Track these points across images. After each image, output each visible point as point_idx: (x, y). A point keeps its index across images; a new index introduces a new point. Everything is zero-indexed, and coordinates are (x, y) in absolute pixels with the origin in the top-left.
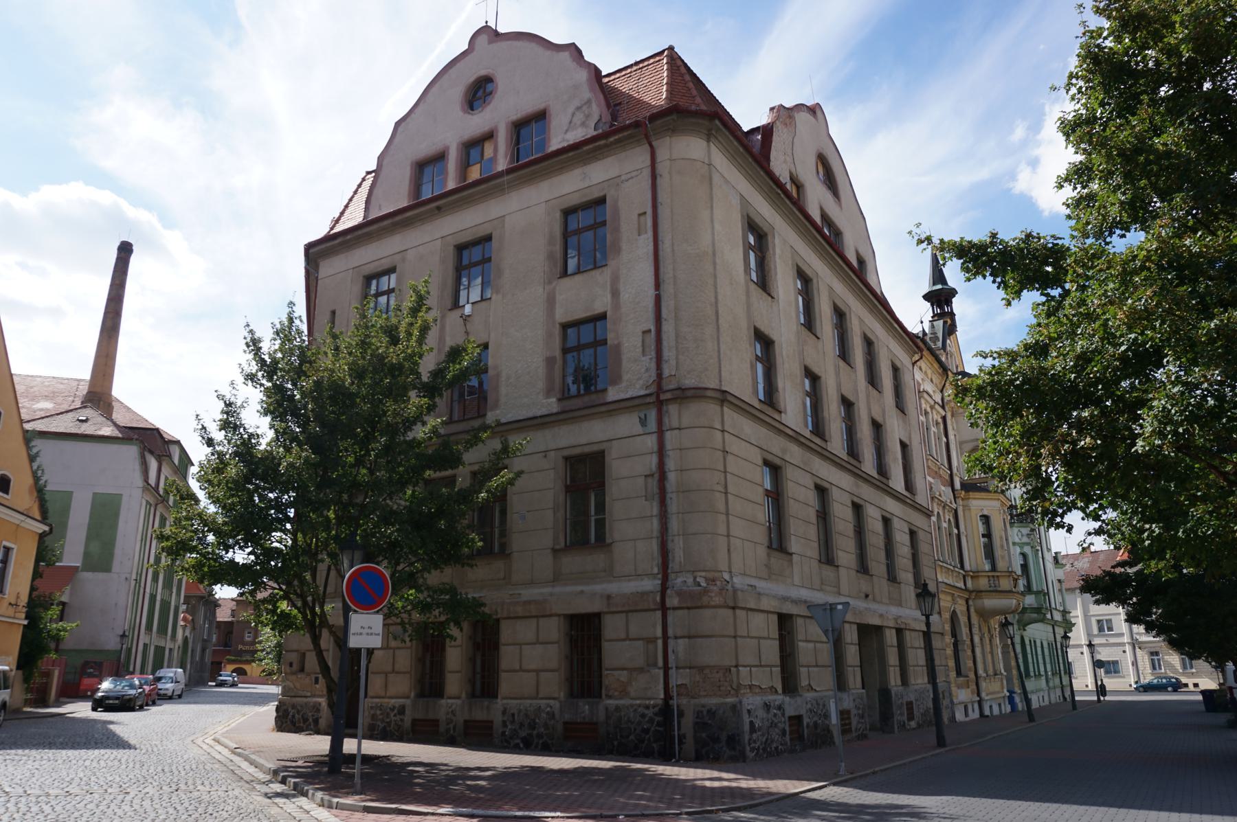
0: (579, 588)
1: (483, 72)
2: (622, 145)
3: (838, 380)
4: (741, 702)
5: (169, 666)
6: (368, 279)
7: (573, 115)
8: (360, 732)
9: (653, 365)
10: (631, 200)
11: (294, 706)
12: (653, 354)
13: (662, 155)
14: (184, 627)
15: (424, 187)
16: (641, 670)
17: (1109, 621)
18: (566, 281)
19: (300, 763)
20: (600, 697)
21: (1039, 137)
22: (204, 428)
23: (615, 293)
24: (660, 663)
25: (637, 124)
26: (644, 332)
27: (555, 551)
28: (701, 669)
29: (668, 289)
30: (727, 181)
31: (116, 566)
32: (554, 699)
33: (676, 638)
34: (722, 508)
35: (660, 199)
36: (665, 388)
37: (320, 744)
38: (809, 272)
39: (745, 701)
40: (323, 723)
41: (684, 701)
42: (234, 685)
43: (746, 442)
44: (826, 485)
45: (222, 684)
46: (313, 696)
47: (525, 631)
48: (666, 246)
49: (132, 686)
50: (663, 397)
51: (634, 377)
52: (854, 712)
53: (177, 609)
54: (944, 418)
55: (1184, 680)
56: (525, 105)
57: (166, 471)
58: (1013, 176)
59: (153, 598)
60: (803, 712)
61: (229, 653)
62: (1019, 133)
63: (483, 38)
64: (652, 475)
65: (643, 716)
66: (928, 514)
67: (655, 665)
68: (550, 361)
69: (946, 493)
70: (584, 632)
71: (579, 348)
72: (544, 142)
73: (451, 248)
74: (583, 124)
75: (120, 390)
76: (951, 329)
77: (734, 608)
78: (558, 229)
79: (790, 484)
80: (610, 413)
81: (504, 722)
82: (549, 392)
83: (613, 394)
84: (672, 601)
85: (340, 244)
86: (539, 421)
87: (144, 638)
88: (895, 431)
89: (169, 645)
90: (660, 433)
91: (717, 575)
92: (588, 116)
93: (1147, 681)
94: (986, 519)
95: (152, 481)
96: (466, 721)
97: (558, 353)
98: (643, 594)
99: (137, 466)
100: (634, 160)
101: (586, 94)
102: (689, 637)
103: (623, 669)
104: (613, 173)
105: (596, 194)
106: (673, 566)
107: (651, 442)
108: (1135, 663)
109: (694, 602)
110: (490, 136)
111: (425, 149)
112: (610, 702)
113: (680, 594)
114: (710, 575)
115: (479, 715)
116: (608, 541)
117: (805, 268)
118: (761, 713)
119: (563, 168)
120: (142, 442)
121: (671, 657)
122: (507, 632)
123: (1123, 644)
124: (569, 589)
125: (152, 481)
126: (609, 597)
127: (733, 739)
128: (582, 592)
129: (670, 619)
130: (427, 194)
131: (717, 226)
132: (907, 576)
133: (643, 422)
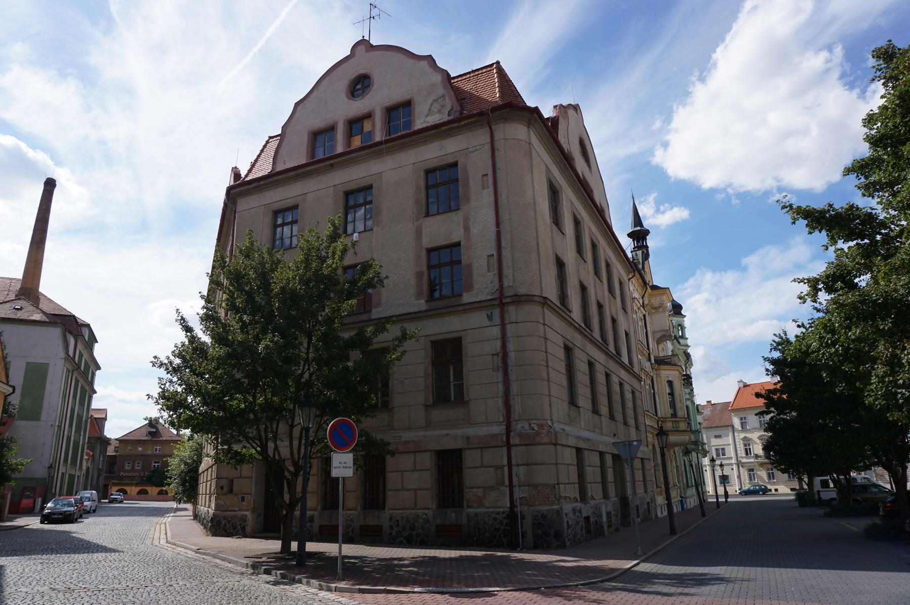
0: (445, 432)
1: (362, 72)
2: (469, 127)
3: (597, 291)
4: (561, 508)
5: (85, 489)
6: (276, 213)
7: (432, 104)
8: (340, 538)
9: (496, 279)
10: (476, 165)
11: (225, 518)
12: (496, 271)
13: (498, 135)
14: (87, 460)
15: (317, 150)
16: (492, 488)
17: (723, 449)
18: (430, 220)
19: (264, 559)
20: (463, 507)
21: (669, 127)
22: (183, 319)
23: (467, 229)
24: (507, 483)
25: (481, 114)
26: (489, 256)
27: (426, 406)
28: (536, 486)
29: (506, 227)
30: (539, 156)
31: (44, 417)
32: (429, 509)
33: (518, 465)
34: (545, 376)
35: (498, 165)
36: (506, 295)
37: (275, 545)
38: (579, 217)
39: (564, 508)
40: (248, 529)
41: (525, 508)
42: (121, 502)
43: (556, 331)
44: (593, 361)
45: (111, 502)
46: (241, 510)
47: (405, 462)
48: (503, 198)
49: (70, 505)
50: (504, 301)
51: (482, 286)
52: (613, 513)
53: (83, 446)
54: (644, 316)
55: (769, 487)
56: (396, 95)
57: (80, 346)
58: (651, 152)
59: (69, 438)
60: (590, 514)
61: (113, 478)
62: (658, 124)
63: (362, 48)
64: (497, 354)
65: (495, 519)
66: (639, 379)
67: (503, 484)
68: (419, 275)
69: (647, 366)
70: (449, 463)
71: (439, 266)
72: (409, 124)
73: (342, 194)
74: (439, 112)
75: (47, 287)
76: (646, 256)
77: (555, 445)
78: (422, 183)
79: (577, 360)
80: (465, 311)
81: (391, 527)
82: (419, 296)
83: (467, 298)
84: (515, 440)
85: (255, 188)
86: (413, 316)
87: (62, 469)
88: (623, 325)
89: (77, 474)
90: (503, 325)
91: (544, 422)
92: (443, 106)
93: (746, 488)
94: (670, 383)
95: (71, 354)
96: (361, 526)
97: (425, 269)
98: (494, 436)
99: (60, 342)
100: (478, 138)
101: (441, 91)
102: (527, 465)
103: (479, 488)
104: (463, 146)
105: (451, 160)
106: (515, 416)
107: (496, 331)
108: (739, 477)
109: (530, 441)
110: (369, 116)
111: (318, 123)
112: (471, 510)
113: (520, 435)
114: (540, 422)
115: (371, 521)
116: (466, 399)
117: (577, 214)
118: (571, 515)
119: (425, 141)
120: (64, 325)
121: (515, 479)
122: (390, 462)
123: (732, 464)
124: (436, 433)
125: (71, 354)
126: (468, 438)
127: (558, 535)
128: (448, 435)
129: (513, 452)
130: (320, 155)
131: (536, 186)
132: (631, 422)
133: (490, 318)
